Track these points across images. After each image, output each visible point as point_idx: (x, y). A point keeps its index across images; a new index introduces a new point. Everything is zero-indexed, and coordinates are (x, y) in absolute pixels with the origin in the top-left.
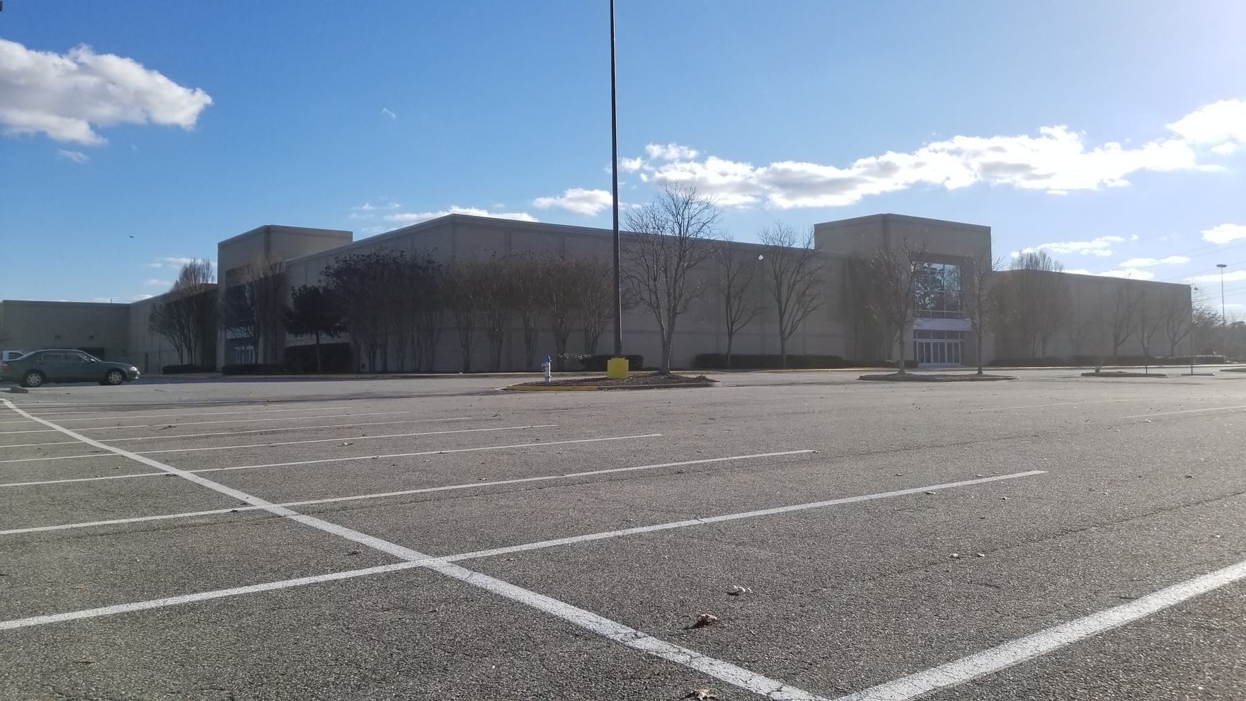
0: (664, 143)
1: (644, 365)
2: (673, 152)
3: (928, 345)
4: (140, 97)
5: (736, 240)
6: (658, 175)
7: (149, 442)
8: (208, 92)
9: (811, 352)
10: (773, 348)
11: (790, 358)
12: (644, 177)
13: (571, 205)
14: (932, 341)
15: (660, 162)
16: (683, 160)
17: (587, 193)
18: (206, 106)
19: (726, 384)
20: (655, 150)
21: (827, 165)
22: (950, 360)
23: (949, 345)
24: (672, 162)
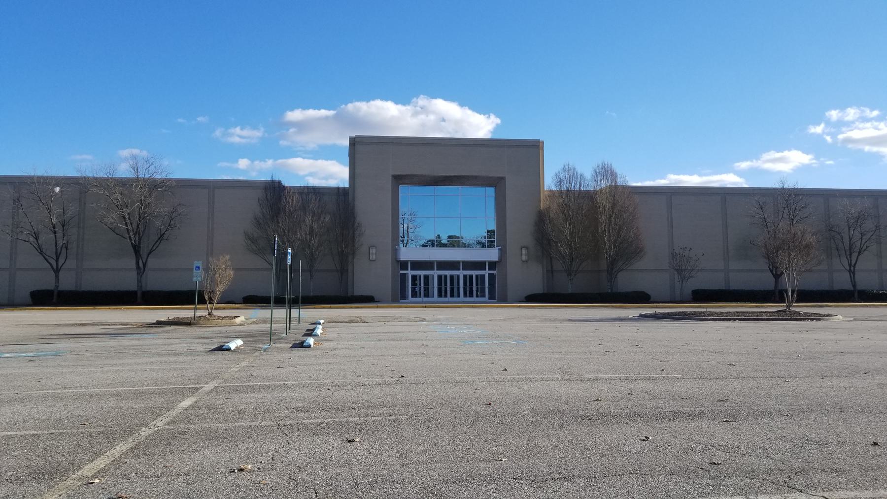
0: (843, 107)
1: (652, 300)
2: (852, 113)
3: (471, 277)
4: (457, 122)
5: (801, 186)
6: (841, 137)
7: (255, 341)
8: (497, 116)
9: (837, 287)
10: (842, 281)
11: (61, 293)
12: (828, 139)
13: (768, 166)
14: (461, 273)
15: (841, 124)
16: (865, 120)
17: (778, 155)
18: (497, 125)
19: (841, 315)
20: (834, 114)
21: (387, 100)
22: (492, 297)
23: (414, 278)
24: (853, 122)
